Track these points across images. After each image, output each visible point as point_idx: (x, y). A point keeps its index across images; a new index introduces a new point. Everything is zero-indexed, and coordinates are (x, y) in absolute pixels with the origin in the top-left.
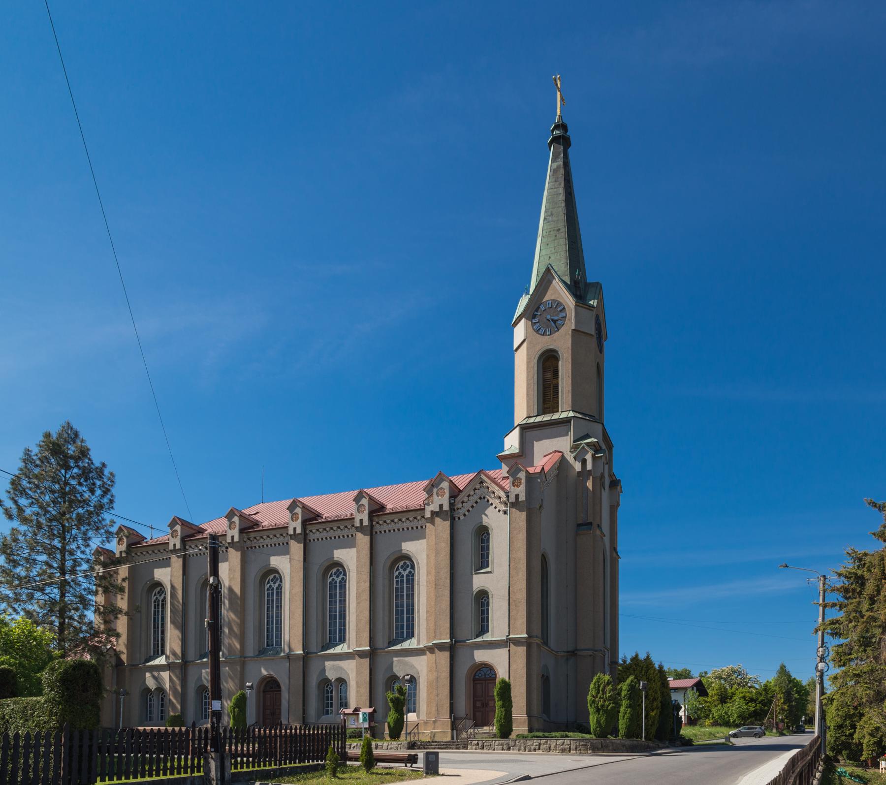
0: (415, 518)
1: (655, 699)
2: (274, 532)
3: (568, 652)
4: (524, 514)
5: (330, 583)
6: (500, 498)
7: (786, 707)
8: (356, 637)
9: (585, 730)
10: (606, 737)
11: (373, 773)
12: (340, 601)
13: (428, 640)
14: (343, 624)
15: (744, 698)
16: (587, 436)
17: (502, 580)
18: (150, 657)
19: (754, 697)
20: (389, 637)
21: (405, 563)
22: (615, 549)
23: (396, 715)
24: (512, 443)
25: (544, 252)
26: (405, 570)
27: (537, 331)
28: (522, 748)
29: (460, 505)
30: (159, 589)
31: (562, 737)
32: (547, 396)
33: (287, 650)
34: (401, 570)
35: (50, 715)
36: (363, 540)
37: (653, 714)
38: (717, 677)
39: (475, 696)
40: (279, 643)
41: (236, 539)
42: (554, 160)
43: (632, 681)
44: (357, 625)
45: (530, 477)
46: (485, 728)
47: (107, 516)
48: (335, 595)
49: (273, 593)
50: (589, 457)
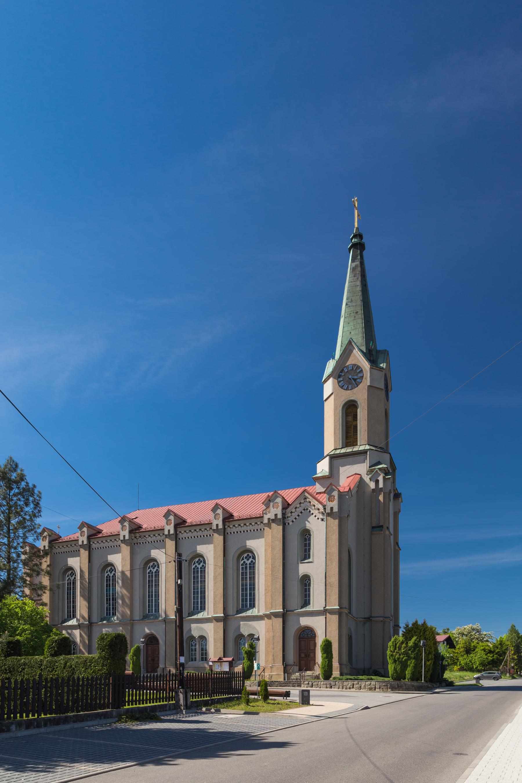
0: (256, 523)
1: (430, 653)
2: (153, 533)
3: (365, 618)
4: (337, 521)
5: (194, 569)
6: (319, 509)
7: (516, 657)
8: (213, 607)
9: (386, 675)
10: (400, 680)
11: (268, 703)
12: (201, 581)
13: (266, 611)
14: (203, 598)
15: (484, 650)
16: (379, 463)
17: (320, 567)
18: (65, 619)
19: (492, 650)
20: (237, 608)
21: (248, 555)
22: (397, 544)
23: (249, 663)
24: (323, 467)
25: (346, 329)
26: (248, 560)
27: (342, 387)
28: (341, 687)
29: (290, 515)
30: (70, 572)
31: (368, 679)
32: (349, 434)
33: (163, 616)
34: (245, 560)
35: (103, 666)
36: (218, 539)
37: (428, 663)
38: (460, 633)
39: (300, 649)
40: (157, 610)
41: (127, 537)
42: (353, 261)
43: (415, 640)
44: (214, 599)
45: (341, 495)
46: (308, 672)
47: (38, 521)
48: (198, 577)
49: (152, 576)
50: (381, 479)
